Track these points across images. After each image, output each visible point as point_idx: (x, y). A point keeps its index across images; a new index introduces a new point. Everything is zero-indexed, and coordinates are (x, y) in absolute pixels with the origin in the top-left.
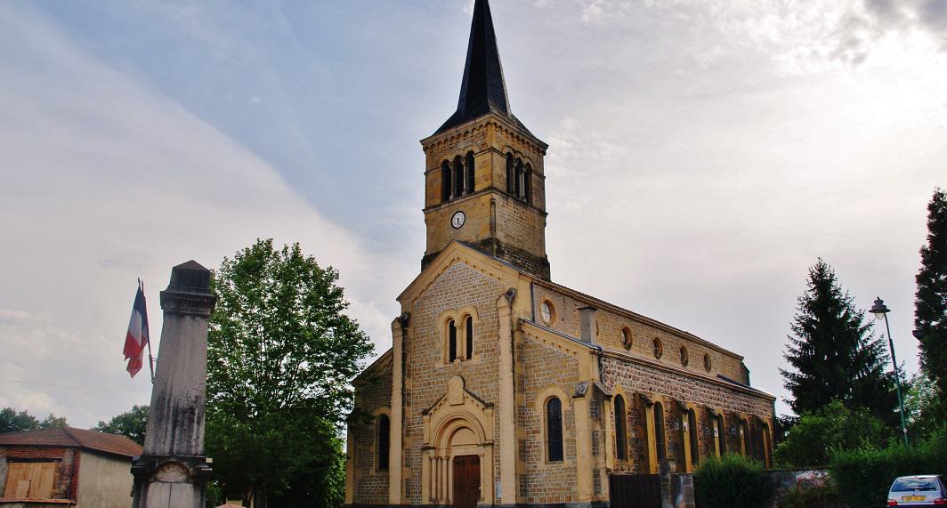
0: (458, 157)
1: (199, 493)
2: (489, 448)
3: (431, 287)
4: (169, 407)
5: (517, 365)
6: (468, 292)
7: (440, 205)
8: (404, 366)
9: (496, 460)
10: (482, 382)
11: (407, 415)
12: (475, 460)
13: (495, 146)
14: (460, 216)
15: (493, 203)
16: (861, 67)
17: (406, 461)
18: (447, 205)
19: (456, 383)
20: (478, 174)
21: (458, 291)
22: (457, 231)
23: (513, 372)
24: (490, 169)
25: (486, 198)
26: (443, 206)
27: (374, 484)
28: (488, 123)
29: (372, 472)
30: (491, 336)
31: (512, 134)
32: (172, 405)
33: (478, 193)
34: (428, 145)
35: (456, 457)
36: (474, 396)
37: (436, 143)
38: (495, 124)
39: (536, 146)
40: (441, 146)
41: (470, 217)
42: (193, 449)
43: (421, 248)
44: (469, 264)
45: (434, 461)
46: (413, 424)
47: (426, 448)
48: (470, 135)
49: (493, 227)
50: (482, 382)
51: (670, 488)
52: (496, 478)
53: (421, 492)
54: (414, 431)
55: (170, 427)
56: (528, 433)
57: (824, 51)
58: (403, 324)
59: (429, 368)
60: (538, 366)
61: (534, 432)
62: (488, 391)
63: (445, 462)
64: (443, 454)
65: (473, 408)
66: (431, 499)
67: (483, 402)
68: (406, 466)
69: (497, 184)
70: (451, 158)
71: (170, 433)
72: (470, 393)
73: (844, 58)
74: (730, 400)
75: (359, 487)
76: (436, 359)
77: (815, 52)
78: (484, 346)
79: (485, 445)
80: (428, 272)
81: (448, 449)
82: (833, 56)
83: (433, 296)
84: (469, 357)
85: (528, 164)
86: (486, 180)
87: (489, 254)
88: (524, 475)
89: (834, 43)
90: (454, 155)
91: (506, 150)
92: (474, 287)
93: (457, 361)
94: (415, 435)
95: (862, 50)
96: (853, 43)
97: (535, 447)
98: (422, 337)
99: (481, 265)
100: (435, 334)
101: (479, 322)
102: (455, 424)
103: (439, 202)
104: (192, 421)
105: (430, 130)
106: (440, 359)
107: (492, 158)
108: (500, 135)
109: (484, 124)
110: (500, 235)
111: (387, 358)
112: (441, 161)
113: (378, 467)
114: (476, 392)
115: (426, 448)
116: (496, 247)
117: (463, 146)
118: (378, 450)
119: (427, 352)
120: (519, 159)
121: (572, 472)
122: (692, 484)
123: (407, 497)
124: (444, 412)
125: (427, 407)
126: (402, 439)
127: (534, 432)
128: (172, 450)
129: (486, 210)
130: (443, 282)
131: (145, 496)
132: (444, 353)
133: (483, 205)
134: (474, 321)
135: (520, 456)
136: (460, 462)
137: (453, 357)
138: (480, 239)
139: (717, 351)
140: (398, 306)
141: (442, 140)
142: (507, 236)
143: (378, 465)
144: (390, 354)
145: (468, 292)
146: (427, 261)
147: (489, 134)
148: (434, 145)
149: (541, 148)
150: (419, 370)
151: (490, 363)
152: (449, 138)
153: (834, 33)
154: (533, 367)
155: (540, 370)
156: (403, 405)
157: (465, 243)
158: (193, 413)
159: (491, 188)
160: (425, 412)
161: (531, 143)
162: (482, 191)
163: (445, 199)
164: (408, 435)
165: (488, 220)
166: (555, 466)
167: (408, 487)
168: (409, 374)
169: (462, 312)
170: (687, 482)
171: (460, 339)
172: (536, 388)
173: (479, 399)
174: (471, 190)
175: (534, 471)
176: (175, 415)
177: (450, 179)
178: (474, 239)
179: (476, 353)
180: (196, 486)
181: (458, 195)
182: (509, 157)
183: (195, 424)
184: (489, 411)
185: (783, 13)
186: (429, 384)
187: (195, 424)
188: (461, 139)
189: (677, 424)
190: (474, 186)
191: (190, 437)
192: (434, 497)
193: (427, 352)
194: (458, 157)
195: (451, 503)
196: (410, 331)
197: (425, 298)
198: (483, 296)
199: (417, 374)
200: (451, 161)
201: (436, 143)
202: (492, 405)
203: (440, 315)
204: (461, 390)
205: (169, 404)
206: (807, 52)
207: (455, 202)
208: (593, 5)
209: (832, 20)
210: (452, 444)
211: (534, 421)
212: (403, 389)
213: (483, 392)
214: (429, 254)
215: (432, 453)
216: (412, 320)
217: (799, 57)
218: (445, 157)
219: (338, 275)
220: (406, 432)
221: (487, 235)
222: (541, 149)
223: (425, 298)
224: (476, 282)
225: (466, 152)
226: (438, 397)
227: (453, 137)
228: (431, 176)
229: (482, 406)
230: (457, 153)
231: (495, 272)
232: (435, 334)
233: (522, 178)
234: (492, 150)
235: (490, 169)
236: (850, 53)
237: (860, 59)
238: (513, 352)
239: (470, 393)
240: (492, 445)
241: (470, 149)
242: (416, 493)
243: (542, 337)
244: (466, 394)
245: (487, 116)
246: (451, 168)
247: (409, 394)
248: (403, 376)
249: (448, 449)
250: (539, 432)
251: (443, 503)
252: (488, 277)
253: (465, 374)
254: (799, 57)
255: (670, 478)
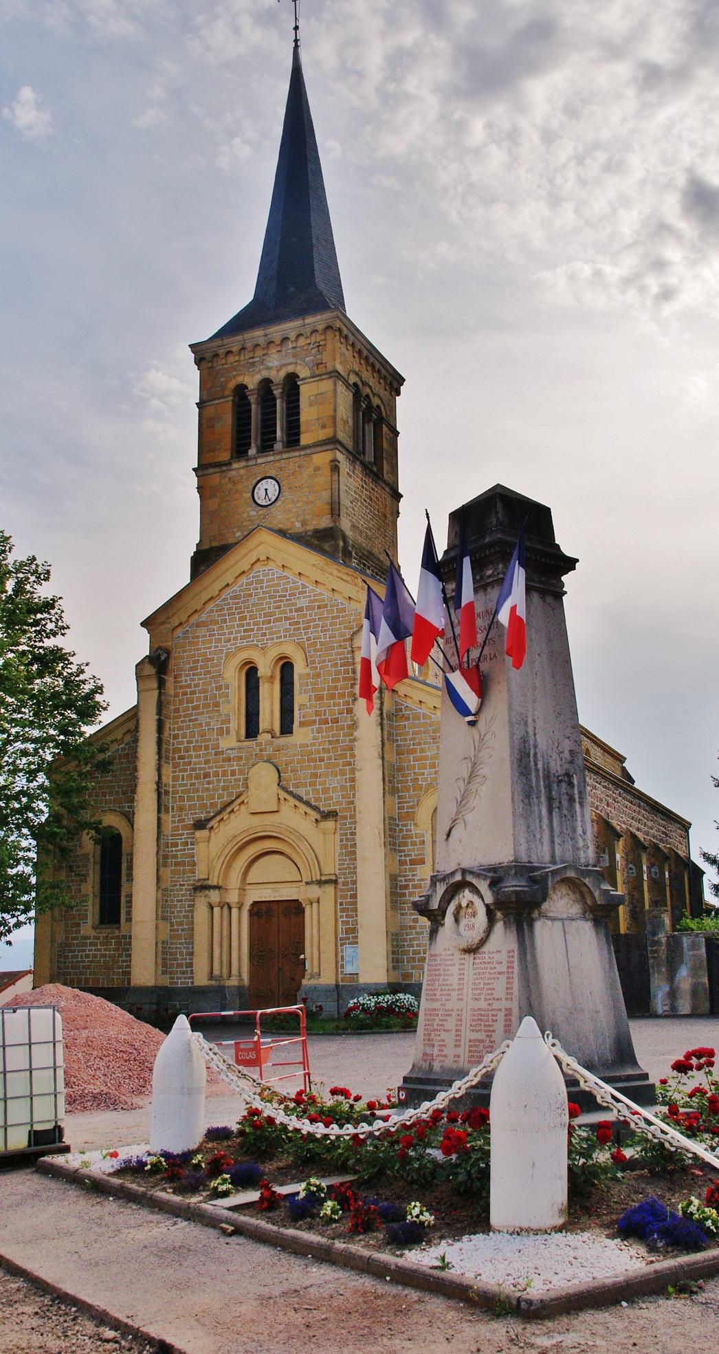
0: (266, 383)
1: (514, 928)
2: (330, 889)
3: (210, 606)
4: (537, 770)
5: (387, 747)
6: (287, 619)
7: (230, 464)
8: (160, 742)
9: (349, 906)
10: (315, 775)
11: (163, 828)
12: (295, 909)
13: (339, 368)
14: (270, 485)
15: (335, 468)
16: (668, 309)
17: (163, 912)
18: (243, 464)
19: (263, 777)
20: (307, 414)
22: (264, 511)
23: (383, 758)
24: (324, 407)
25: (322, 458)
26: (235, 466)
27: (90, 950)
28: (329, 327)
29: (87, 929)
30: (332, 696)
31: (360, 352)
32: (540, 766)
33: (305, 448)
34: (204, 354)
35: (255, 903)
36: (300, 799)
37: (222, 352)
38: (340, 330)
39: (389, 378)
40: (231, 359)
41: (290, 487)
42: (582, 854)
43: (189, 538)
44: (276, 565)
45: (216, 910)
46: (176, 845)
47: (202, 887)
48: (290, 345)
49: (335, 509)
50: (315, 775)
51: (664, 957)
52: (350, 934)
53: (191, 965)
54: (175, 857)
55: (544, 812)
56: (402, 863)
57: (613, 272)
58: (157, 667)
59: (207, 748)
60: (422, 751)
61: (413, 862)
62: (326, 790)
63: (235, 912)
64: (233, 897)
65: (294, 819)
66: (211, 976)
67: (316, 808)
68: (164, 918)
69: (341, 436)
70: (252, 381)
71: (545, 821)
72: (290, 793)
73: (643, 289)
74: (650, 824)
75: (59, 956)
76: (221, 732)
77: (598, 274)
78: (317, 713)
79: (321, 883)
80: (206, 581)
81: (242, 890)
82: (626, 282)
83: (217, 622)
84: (286, 728)
85: (378, 407)
86: (324, 427)
87: (331, 555)
88: (397, 935)
89: (629, 262)
90: (258, 378)
91: (353, 379)
92: (300, 609)
93: (263, 738)
94: (176, 864)
95: (673, 280)
96: (660, 265)
97: (415, 887)
98: (193, 693)
99: (315, 575)
100: (219, 688)
101: (308, 670)
102: (265, 846)
103: (225, 456)
104: (571, 799)
105: (206, 330)
106: (228, 732)
107: (335, 390)
108: (344, 350)
109: (320, 327)
110: (345, 524)
111: (122, 724)
112: (232, 385)
113: (97, 922)
114: (301, 792)
115: (202, 887)
116: (341, 544)
117: (276, 363)
118: (97, 891)
119: (203, 719)
120: (367, 396)
121: (125, 945)
122: (703, 950)
123: (164, 973)
124: (238, 824)
125: (203, 816)
126: (158, 870)
127: (413, 862)
128: (553, 856)
129: (324, 477)
131: (532, 938)
132: (238, 723)
133: (317, 469)
134: (299, 669)
135: (392, 901)
136: (260, 911)
137: (252, 730)
138: (310, 528)
139: (599, 746)
140: (145, 635)
141: (234, 349)
142: (354, 526)
143: (97, 917)
144: (132, 716)
145: (287, 619)
146: (203, 560)
147: (329, 347)
148: (217, 355)
149: (394, 381)
150: (187, 750)
151: (330, 742)
152: (249, 345)
153: (629, 246)
154: (414, 751)
155: (426, 758)
156: (159, 811)
157: (282, 533)
158: (571, 784)
159: (333, 442)
160: (200, 825)
161: (383, 371)
162: (315, 445)
163: (240, 450)
164: (165, 865)
165: (326, 495)
166: (105, 932)
167: (166, 956)
168: (167, 758)
169: (274, 653)
170: (694, 946)
171: (266, 703)
172: (417, 787)
173: (307, 804)
174: (293, 440)
175: (414, 928)
176: (549, 788)
177: (244, 422)
178: (298, 527)
179: (302, 724)
180: (597, 923)
181: (267, 446)
182: (357, 396)
183: (577, 806)
184: (329, 825)
185: (555, 201)
186: (206, 775)
187: (577, 806)
188: (273, 350)
189: (606, 857)
190: (298, 434)
191: (574, 830)
192: (216, 972)
193: (203, 719)
194: (266, 383)
195: (246, 982)
196: (170, 681)
197: (198, 625)
198: (317, 626)
199: (181, 758)
200: (251, 387)
201: (222, 352)
202: (330, 815)
205: (536, 765)
206: (587, 270)
207: (260, 461)
208: (237, 141)
209: (629, 223)
210: (250, 879)
211: (414, 844)
212: (159, 783)
213: (316, 791)
214: (206, 547)
215: (214, 896)
216: (172, 662)
217: (572, 278)
218: (240, 380)
219: (48, 572)
220: (162, 860)
221: (325, 522)
222: (395, 385)
224: (303, 602)
225: (283, 374)
226: (229, 800)
227: (230, 352)
228: (210, 411)
229: (314, 815)
230: (265, 374)
231: (339, 585)
232: (219, 688)
233: (369, 429)
234: (335, 374)
235: (324, 407)
236: (653, 284)
237: (667, 294)
238: (381, 725)
239: (290, 793)
240: (336, 882)
241: (291, 369)
242: (180, 965)
243: (417, 695)
244: (283, 795)
245: (327, 315)
246: (277, 392)
247: (167, 793)
248: (160, 759)
249: (242, 890)
250: (422, 862)
251: (233, 982)
252: (327, 595)
253: (281, 759)
254: (572, 278)
255: (664, 940)
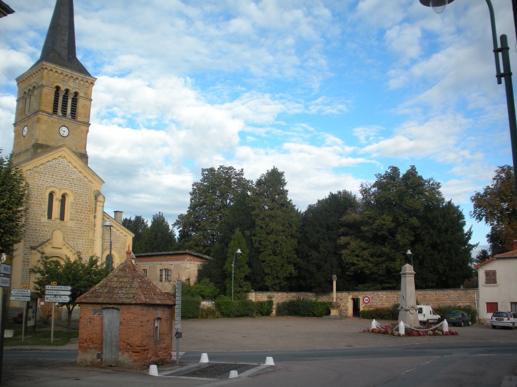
3: (41, 167)
4: (31, 350)
6: (68, 181)
10: (74, 238)
21: (62, 177)
30: (81, 212)
62: (77, 244)
76: (42, 215)
92: (73, 179)
100: (42, 198)
130: (50, 166)
141: (59, 72)
145: (68, 181)
151: (80, 228)
152: (65, 74)
197: (36, 172)
198: (78, 187)
203: (47, 188)
204: (62, 240)
213: (74, 244)
223: (36, 172)
224: (74, 177)
252: (82, 177)
